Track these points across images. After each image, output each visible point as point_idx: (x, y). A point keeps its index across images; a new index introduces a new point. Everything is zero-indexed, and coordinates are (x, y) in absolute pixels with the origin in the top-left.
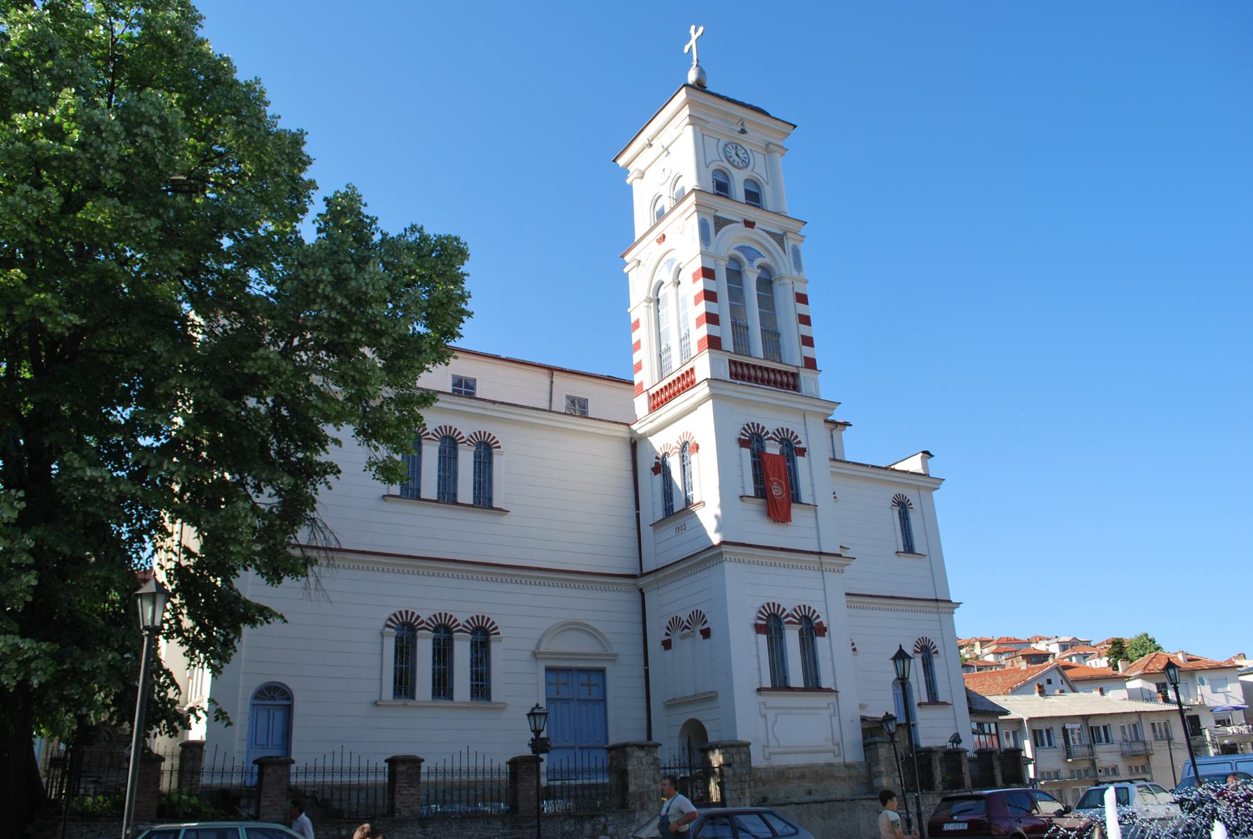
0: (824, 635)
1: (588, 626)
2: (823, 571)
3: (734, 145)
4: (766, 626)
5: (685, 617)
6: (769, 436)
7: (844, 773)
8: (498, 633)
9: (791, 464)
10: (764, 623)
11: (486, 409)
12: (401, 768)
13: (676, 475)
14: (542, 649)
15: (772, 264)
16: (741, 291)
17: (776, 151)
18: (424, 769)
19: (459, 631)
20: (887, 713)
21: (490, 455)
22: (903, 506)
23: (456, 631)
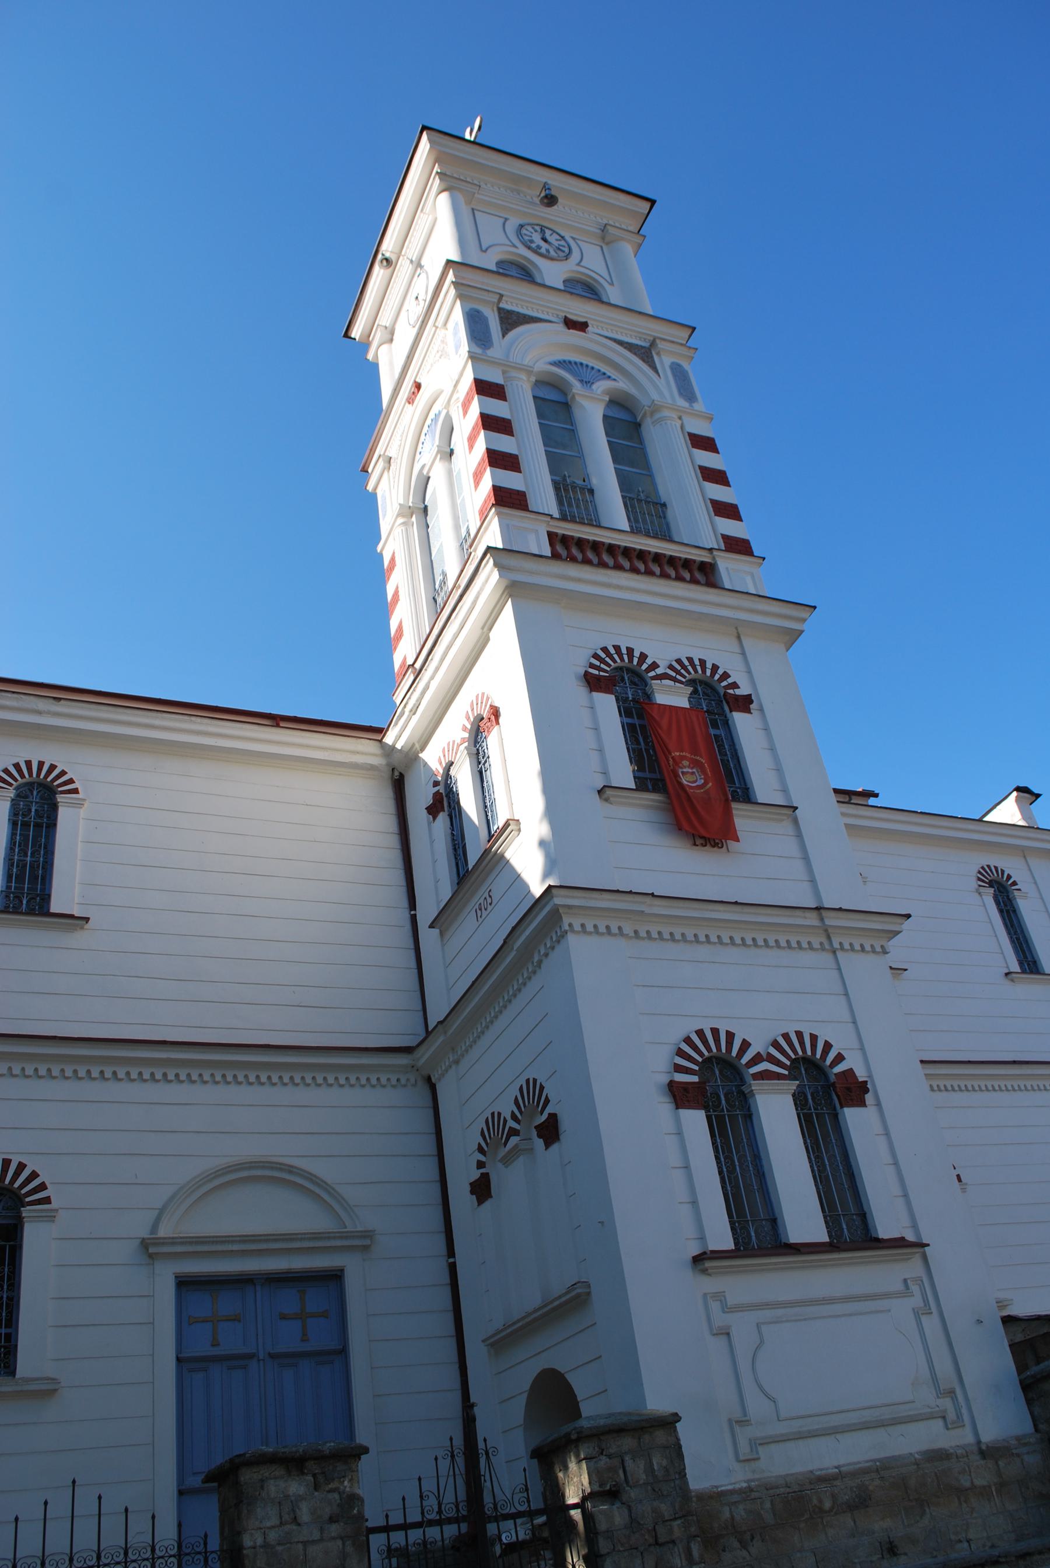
0: (862, 1103)
1: (290, 1169)
2: (834, 952)
3: (538, 228)
4: (699, 1087)
6: (659, 671)
7: (983, 1476)
9: (721, 732)
10: (695, 1079)
11: (40, 713)
13: (468, 802)
14: (162, 1233)
15: (633, 391)
16: (572, 432)
17: (622, 239)
21: (52, 809)
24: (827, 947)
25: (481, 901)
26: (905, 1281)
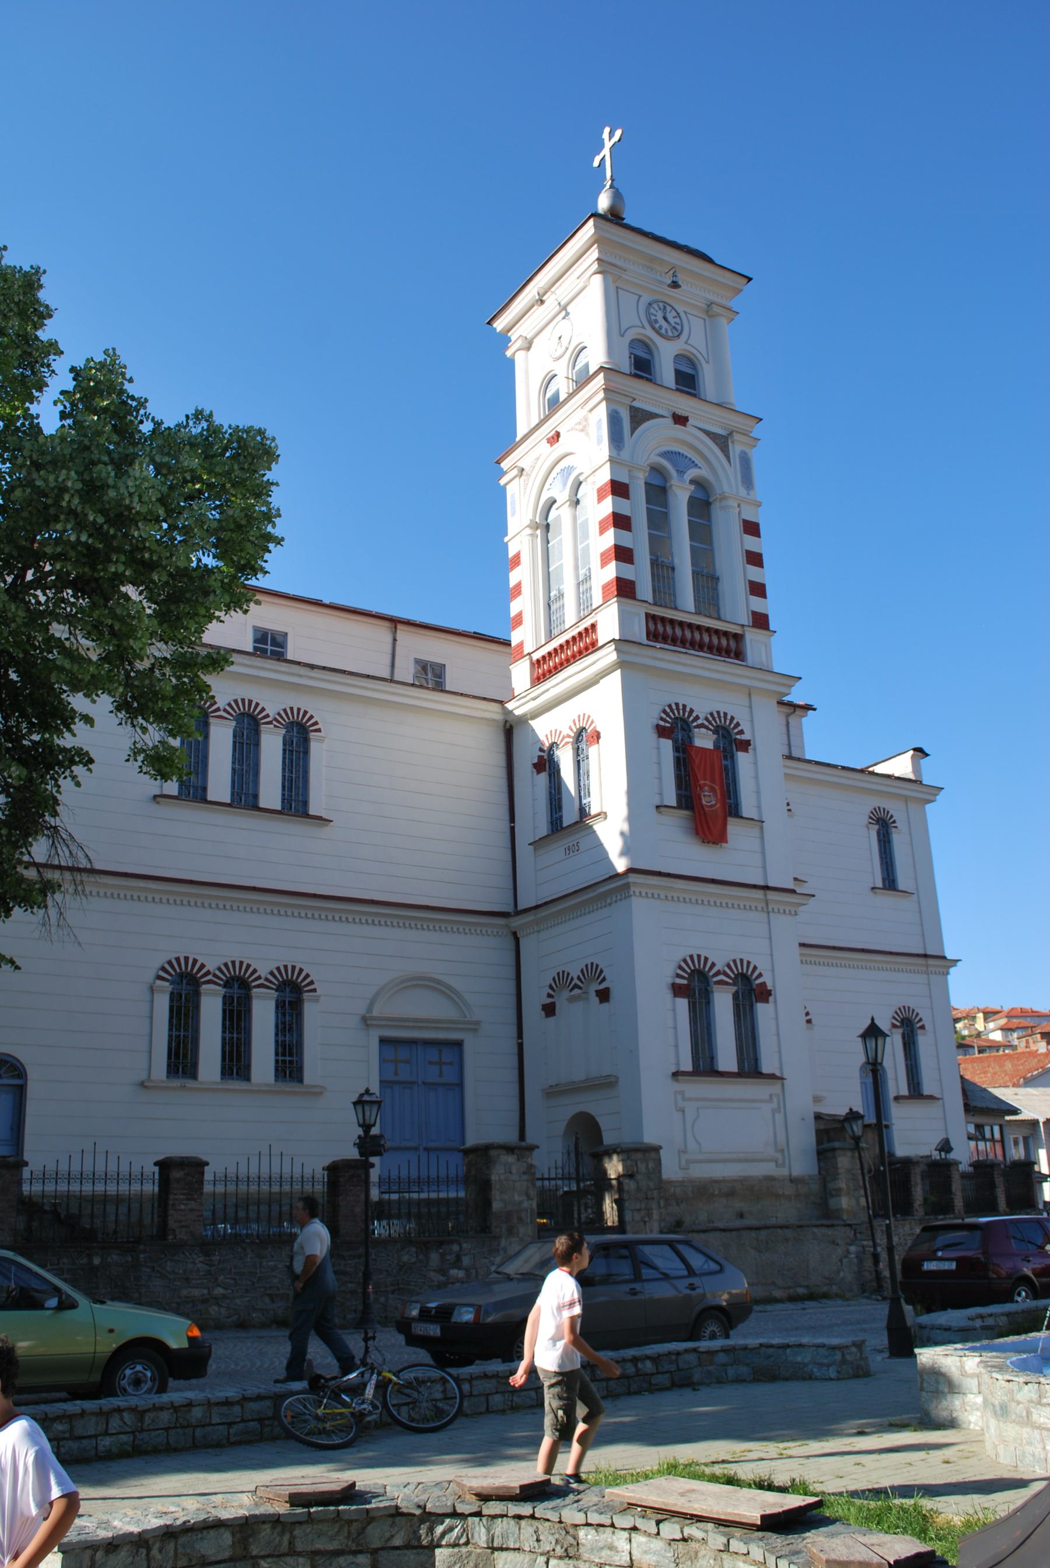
0: (767, 1001)
1: (438, 982)
4: (687, 986)
5: (575, 973)
6: (699, 722)
8: (314, 990)
10: (685, 982)
12: (176, 1174)
14: (375, 1013)
17: (722, 315)
18: (208, 1176)
19: (259, 986)
20: (851, 1109)
21: (306, 741)
22: (883, 825)
23: (255, 987)
24: (765, 910)
25: (571, 844)
26: (771, 1095)
